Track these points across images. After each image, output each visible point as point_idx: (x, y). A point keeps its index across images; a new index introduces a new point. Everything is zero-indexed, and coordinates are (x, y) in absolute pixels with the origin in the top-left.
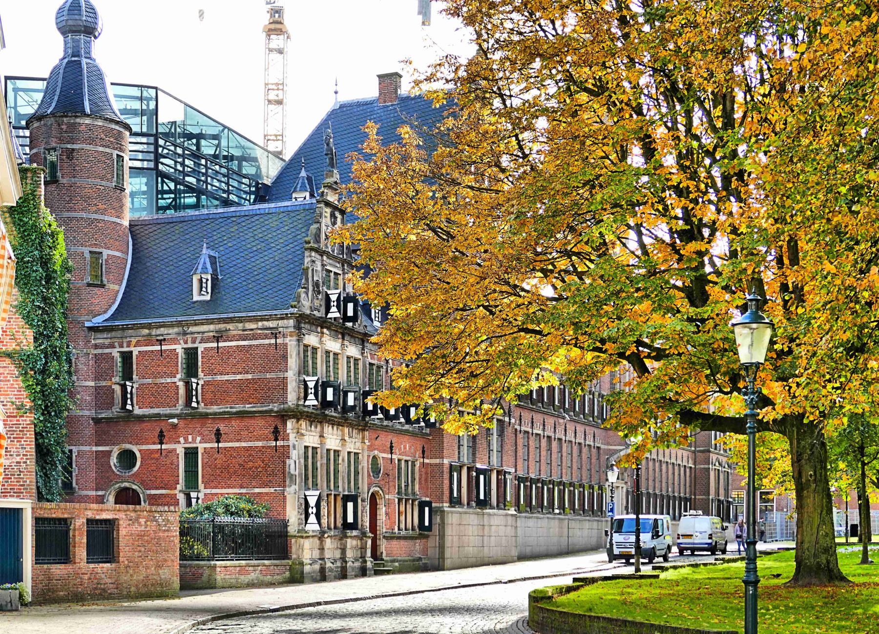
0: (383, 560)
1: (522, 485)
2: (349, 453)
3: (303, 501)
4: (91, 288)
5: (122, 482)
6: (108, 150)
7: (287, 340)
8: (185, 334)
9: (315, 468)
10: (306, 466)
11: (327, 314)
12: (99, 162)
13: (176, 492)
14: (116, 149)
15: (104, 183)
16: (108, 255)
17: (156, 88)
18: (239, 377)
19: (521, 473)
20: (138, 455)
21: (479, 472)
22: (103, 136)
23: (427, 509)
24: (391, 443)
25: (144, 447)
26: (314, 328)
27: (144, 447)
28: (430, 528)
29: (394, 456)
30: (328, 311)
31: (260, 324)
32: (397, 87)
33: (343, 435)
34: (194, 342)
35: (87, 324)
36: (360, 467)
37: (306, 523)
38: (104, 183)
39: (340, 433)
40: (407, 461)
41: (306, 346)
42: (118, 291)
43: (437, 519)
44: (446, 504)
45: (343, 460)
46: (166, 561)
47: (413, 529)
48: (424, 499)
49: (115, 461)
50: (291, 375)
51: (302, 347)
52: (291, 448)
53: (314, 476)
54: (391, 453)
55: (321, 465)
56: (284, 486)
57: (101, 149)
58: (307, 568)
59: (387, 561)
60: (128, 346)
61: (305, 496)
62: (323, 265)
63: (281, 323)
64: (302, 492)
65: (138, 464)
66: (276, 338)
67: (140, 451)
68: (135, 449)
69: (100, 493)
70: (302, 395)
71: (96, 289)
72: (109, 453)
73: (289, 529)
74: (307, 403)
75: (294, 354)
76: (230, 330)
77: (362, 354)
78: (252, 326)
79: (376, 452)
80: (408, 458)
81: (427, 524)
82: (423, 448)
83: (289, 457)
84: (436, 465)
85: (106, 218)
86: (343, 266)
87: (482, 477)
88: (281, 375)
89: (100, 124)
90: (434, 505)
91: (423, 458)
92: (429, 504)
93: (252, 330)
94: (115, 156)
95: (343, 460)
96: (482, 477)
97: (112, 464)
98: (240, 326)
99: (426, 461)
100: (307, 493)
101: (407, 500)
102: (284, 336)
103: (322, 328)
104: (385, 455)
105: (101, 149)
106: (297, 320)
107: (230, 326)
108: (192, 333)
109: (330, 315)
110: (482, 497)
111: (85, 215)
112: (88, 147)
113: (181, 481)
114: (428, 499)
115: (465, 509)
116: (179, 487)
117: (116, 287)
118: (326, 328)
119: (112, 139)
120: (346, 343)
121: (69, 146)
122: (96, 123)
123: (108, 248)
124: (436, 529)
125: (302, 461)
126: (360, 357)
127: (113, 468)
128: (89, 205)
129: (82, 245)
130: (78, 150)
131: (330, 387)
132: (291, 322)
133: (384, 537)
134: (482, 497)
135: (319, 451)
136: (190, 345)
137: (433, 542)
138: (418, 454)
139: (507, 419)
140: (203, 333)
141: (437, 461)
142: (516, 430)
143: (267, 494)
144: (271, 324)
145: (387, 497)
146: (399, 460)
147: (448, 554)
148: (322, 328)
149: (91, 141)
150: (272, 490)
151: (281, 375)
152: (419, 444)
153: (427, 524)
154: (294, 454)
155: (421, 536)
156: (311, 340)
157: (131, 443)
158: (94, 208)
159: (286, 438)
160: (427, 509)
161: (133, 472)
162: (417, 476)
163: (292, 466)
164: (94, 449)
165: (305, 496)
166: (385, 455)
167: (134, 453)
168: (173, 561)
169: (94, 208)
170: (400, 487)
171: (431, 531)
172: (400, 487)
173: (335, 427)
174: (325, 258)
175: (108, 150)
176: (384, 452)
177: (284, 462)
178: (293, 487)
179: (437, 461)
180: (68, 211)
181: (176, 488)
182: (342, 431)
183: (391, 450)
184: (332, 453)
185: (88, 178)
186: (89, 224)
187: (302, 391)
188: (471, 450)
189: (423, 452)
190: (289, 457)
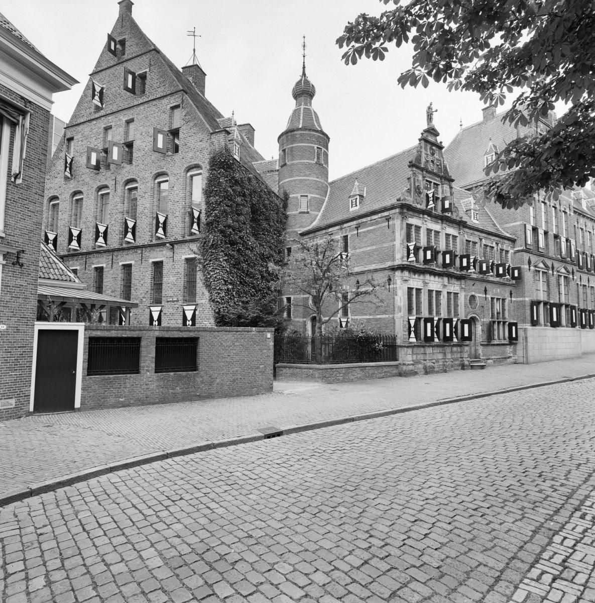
0: (480, 358)
1: (583, 314)
6: (311, 145)
8: (341, 229)
11: (427, 206)
18: (369, 248)
19: (582, 307)
21: (552, 305)
24: (486, 288)
28: (516, 338)
29: (487, 296)
30: (427, 205)
34: (346, 233)
37: (409, 338)
42: (317, 215)
43: (521, 333)
47: (505, 339)
48: (512, 321)
51: (405, 226)
52: (398, 289)
54: (486, 294)
61: (409, 319)
62: (424, 177)
69: (305, 319)
70: (406, 254)
74: (410, 260)
79: (473, 293)
82: (511, 291)
83: (397, 295)
84: (520, 301)
85: (310, 178)
86: (441, 179)
87: (554, 309)
92: (515, 324)
94: (316, 148)
95: (444, 297)
96: (554, 309)
101: (499, 323)
104: (481, 295)
107: (364, 220)
108: (345, 228)
109: (429, 207)
110: (555, 319)
114: (515, 321)
115: (543, 327)
123: (311, 193)
124: (520, 339)
131: (465, 267)
132: (397, 210)
133: (481, 345)
134: (555, 319)
136: (345, 235)
139: (571, 276)
140: (350, 226)
141: (521, 299)
142: (577, 284)
143: (384, 319)
144: (386, 214)
145: (482, 320)
147: (530, 353)
150: (387, 316)
153: (514, 336)
155: (511, 344)
156: (414, 221)
159: (395, 283)
163: (399, 300)
164: (302, 296)
166: (481, 295)
171: (517, 340)
174: (425, 172)
175: (311, 145)
176: (480, 293)
177: (394, 298)
179: (521, 299)
184: (434, 294)
188: (546, 293)
189: (511, 294)
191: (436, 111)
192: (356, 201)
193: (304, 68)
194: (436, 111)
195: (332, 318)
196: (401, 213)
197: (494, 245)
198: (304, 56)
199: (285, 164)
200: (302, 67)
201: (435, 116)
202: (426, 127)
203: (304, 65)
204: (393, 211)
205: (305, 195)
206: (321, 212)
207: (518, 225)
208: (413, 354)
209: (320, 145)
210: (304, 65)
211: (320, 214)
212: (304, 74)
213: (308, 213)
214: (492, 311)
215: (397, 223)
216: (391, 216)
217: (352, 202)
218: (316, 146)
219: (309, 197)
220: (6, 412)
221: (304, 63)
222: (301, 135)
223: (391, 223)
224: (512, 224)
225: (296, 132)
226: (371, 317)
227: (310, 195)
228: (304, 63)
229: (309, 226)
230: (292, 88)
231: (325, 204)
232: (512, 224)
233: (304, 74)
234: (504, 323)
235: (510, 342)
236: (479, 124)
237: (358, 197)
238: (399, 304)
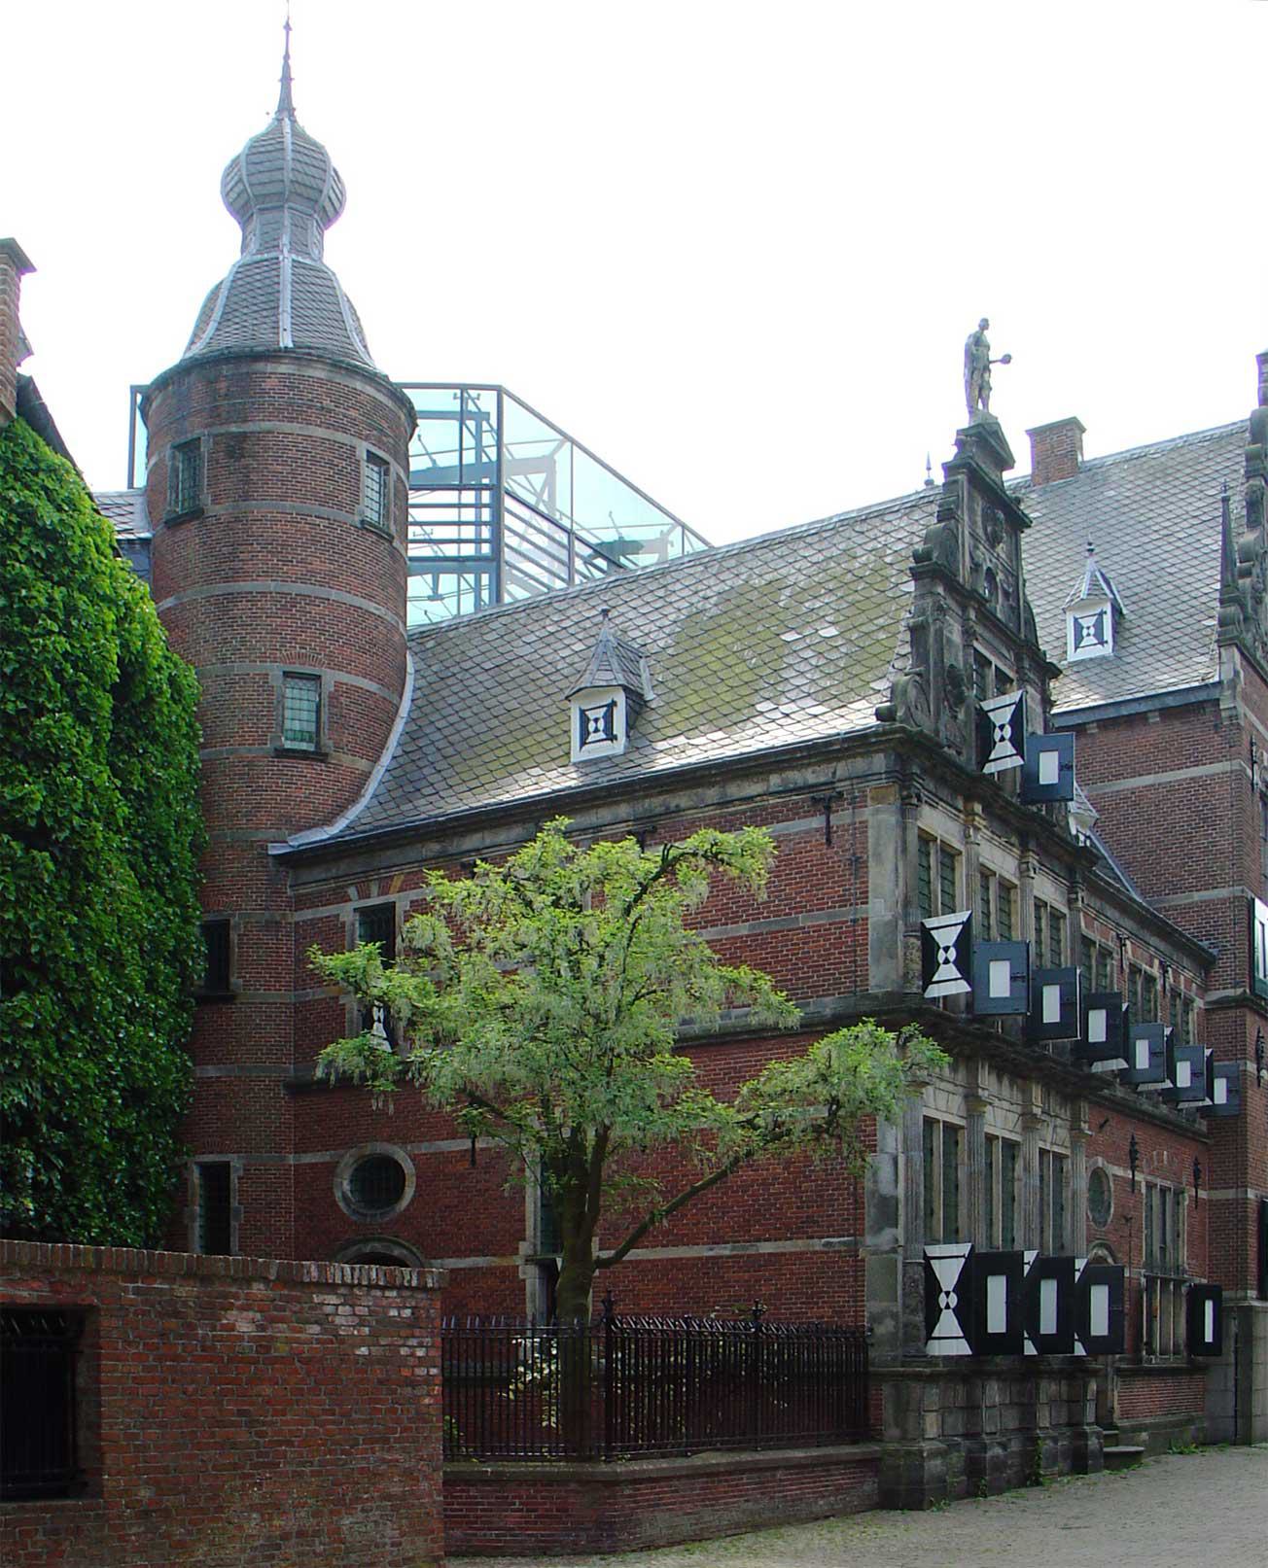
2: (1043, 1152)
3: (919, 1273)
4: (286, 762)
5: (367, 1241)
6: (340, 437)
7: (866, 814)
9: (952, 1187)
10: (928, 1176)
12: (314, 462)
13: (518, 1261)
14: (367, 438)
15: (325, 511)
16: (338, 684)
17: (500, 391)
20: (408, 1167)
22: (327, 403)
23: (1209, 1306)
24: (1133, 1138)
25: (425, 1148)
26: (944, 793)
27: (425, 1148)
28: (1216, 1348)
29: (1139, 1177)
31: (775, 780)
32: (1076, 447)
33: (1027, 1103)
35: (276, 850)
36: (1067, 1194)
38: (325, 511)
39: (1017, 1096)
40: (1164, 1191)
41: (925, 839)
44: (1252, 1293)
45: (1027, 1169)
46: (374, 1476)
49: (346, 1186)
50: (880, 909)
53: (951, 1206)
55: (970, 1175)
56: (859, 1233)
57: (320, 432)
58: (935, 1466)
59: (1123, 1430)
60: (384, 892)
63: (842, 769)
64: (919, 1247)
65: (409, 1192)
66: (828, 810)
67: (414, 1158)
68: (401, 1155)
70: (917, 967)
71: (302, 766)
72: (330, 1169)
73: (872, 1353)
75: (889, 852)
76: (678, 810)
77: (1070, 903)
78: (753, 788)
79: (1100, 1161)
80: (1168, 1184)
81: (1209, 1338)
83: (873, 1148)
84: (1227, 1203)
85: (334, 595)
88: (847, 914)
89: (322, 374)
90: (1225, 1294)
91: (1196, 1187)
93: (751, 799)
95: (1027, 1169)
97: (338, 1195)
98: (712, 794)
99: (1203, 1194)
100: (933, 1250)
102: (857, 803)
103: (968, 799)
104: (1119, 1172)
105: (320, 432)
106: (899, 756)
107: (682, 800)
111: (272, 586)
112: (287, 427)
113: (529, 1232)
116: (524, 1248)
117: (362, 764)
118: (981, 800)
119: (353, 413)
120: (1033, 860)
121: (234, 429)
122: (310, 372)
123: (339, 667)
124: (1229, 1346)
125: (918, 1156)
126: (1065, 910)
127: (341, 1204)
128: (286, 562)
129: (263, 658)
130: (259, 436)
132: (879, 762)
135: (963, 1138)
137: (1223, 1376)
138: (1187, 1177)
143: (799, 1255)
144: (810, 776)
146: (1150, 1186)
148: (968, 799)
149: (295, 412)
150: (817, 1244)
151: (847, 914)
152: (1188, 1153)
154: (891, 1139)
155: (1193, 1370)
157: (389, 1141)
158: (299, 569)
160: (1209, 1306)
161: (392, 1215)
162: (1184, 1228)
165: (928, 1259)
166: (1119, 1172)
167: (398, 1167)
168: (408, 1474)
169: (299, 569)
170: (1150, 1254)
172: (1150, 1254)
173: (1006, 1082)
175: (340, 437)
176: (1117, 1162)
178: (888, 1234)
180: (226, 580)
181: (516, 1251)
182: (1025, 1092)
183: (1133, 1159)
185: (283, 498)
186: (284, 608)
187: (916, 955)
189: (1197, 1174)
190: (873, 1148)
191: (1006, 360)
192: (609, 718)
193: (286, 79)
194: (1006, 360)
195: (634, 1254)
196: (901, 778)
197: (1156, 971)
198: (288, 27)
199: (196, 514)
200: (279, 75)
201: (997, 375)
202: (964, 422)
203: (286, 68)
204: (859, 765)
205: (308, 670)
206: (386, 760)
207: (1223, 901)
208: (1004, 1432)
209: (379, 444)
210: (286, 68)
211: (379, 772)
212: (286, 107)
213: (319, 756)
214: (1042, 1238)
215: (880, 819)
216: (841, 786)
217: (584, 720)
218: (362, 448)
219: (328, 686)
220: (838, 1215)
221: (287, 57)
222: (290, 383)
223: (841, 818)
224: (1197, 896)
225: (260, 366)
226: (725, 1250)
227: (331, 677)
228: (287, 57)
229: (328, 820)
230: (233, 155)
231: (399, 726)
232: (1197, 896)
233: (286, 107)
234: (1178, 1283)
235: (1190, 1361)
236: (1221, 438)
237: (621, 698)
238: (886, 1188)
